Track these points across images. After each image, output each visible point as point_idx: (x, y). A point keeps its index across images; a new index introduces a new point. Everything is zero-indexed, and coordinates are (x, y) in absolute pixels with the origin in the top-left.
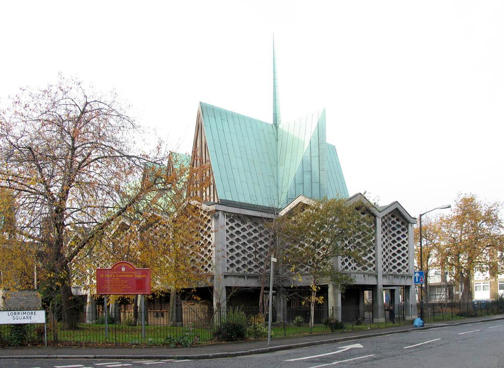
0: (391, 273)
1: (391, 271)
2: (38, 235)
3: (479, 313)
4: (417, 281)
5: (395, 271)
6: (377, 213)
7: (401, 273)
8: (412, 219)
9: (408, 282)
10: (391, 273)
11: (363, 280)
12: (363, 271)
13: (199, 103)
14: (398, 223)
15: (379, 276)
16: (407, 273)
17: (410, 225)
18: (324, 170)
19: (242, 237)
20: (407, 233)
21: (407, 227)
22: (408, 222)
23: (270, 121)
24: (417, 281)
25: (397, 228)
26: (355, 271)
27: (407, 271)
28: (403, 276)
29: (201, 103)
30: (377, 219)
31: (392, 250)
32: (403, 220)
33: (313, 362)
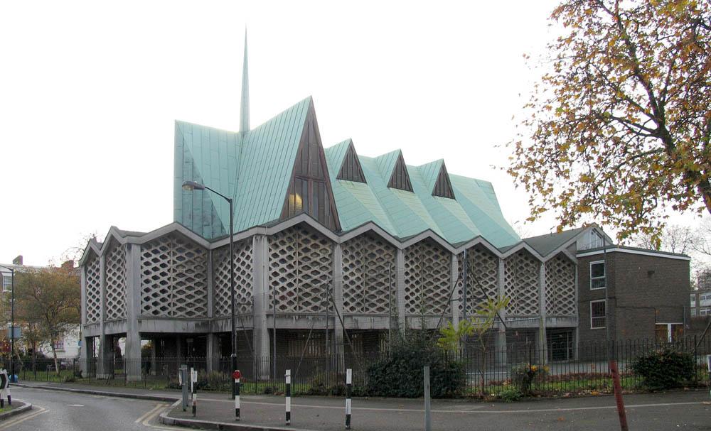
6: (451, 249)
13: (174, 122)
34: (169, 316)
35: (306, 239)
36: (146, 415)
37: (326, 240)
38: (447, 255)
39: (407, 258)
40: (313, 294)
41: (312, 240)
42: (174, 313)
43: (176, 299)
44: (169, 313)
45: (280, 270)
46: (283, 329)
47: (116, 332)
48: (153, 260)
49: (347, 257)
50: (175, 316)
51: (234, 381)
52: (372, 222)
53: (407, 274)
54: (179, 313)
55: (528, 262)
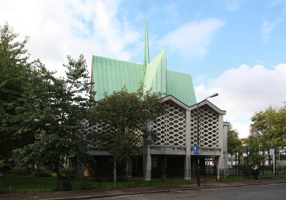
0: (203, 147)
1: (203, 146)
2: (48, 133)
3: (198, 181)
4: (195, 153)
5: (207, 146)
6: (187, 108)
7: (211, 147)
8: (220, 111)
9: (217, 153)
10: (203, 147)
11: (172, 152)
12: (209, 147)
13: (92, 56)
14: (209, 114)
15: (187, 149)
16: (184, 146)
17: (220, 116)
18: (164, 86)
19: (160, 134)
20: (217, 121)
21: (218, 117)
22: (219, 114)
23: (142, 63)
24: (195, 153)
25: (179, 112)
26: (168, 146)
27: (217, 146)
28: (211, 150)
29: (93, 56)
30: (187, 112)
31: (153, 128)
32: (214, 113)
33: (81, 198)
34: (165, 146)
35: (206, 113)
36: (131, 193)
37: (182, 109)
38: (184, 111)
39: (192, 116)
40: (175, 137)
41: (170, 107)
42: (168, 144)
43: (169, 136)
44: (165, 144)
45: (161, 123)
46: (163, 155)
47: (204, 155)
48: (209, 125)
49: (193, 119)
50: (168, 146)
51: (86, 177)
52: (170, 95)
53: (192, 125)
54: (170, 144)
55: (177, 110)
